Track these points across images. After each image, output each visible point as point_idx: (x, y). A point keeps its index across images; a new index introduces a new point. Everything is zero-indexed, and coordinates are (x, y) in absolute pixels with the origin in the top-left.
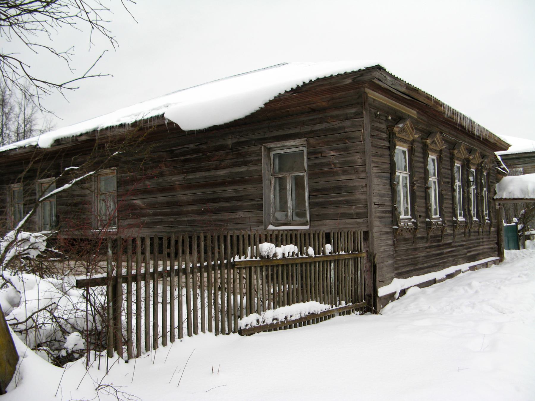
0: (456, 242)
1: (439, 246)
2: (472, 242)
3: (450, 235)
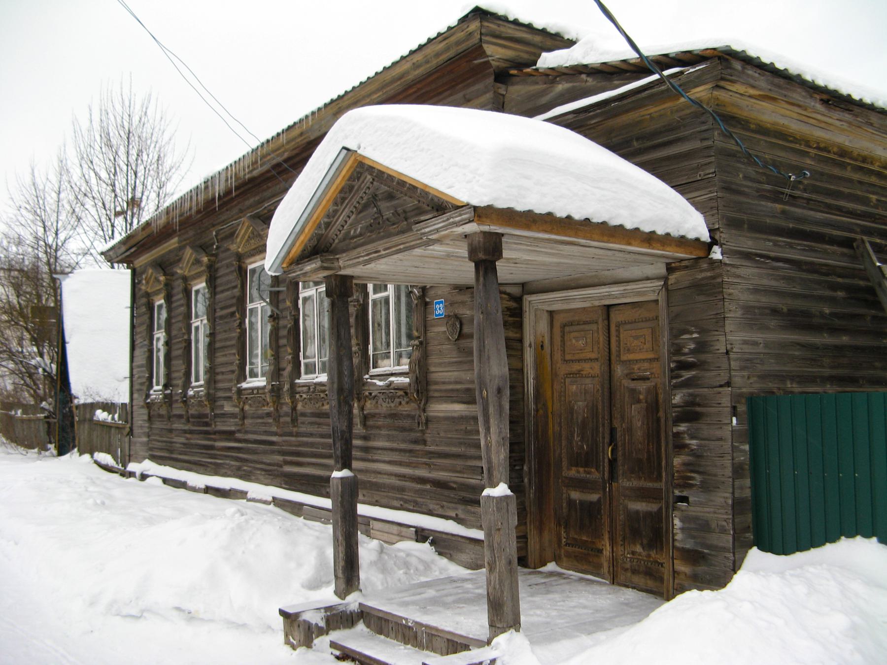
0: (246, 432)
1: (207, 433)
2: (305, 439)
3: (233, 416)
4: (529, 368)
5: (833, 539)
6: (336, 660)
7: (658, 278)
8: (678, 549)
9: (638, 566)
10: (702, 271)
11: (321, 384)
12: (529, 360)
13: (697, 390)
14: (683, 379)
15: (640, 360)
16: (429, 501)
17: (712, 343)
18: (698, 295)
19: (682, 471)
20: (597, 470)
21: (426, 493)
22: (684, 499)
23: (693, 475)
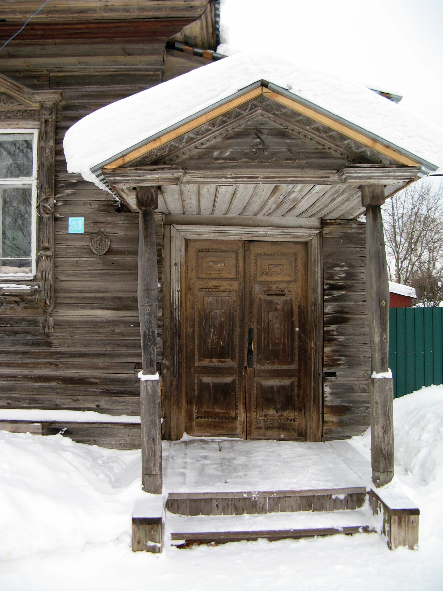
4: (174, 282)
5: (417, 388)
6: (178, 549)
7: (316, 228)
8: (328, 407)
9: (272, 424)
10: (352, 228)
11: (36, 288)
12: (174, 276)
13: (345, 303)
14: (334, 296)
15: (279, 282)
16: (55, 397)
17: (358, 274)
18: (349, 243)
19: (331, 356)
20: (232, 359)
21: (50, 390)
22: (333, 374)
23: (339, 358)
